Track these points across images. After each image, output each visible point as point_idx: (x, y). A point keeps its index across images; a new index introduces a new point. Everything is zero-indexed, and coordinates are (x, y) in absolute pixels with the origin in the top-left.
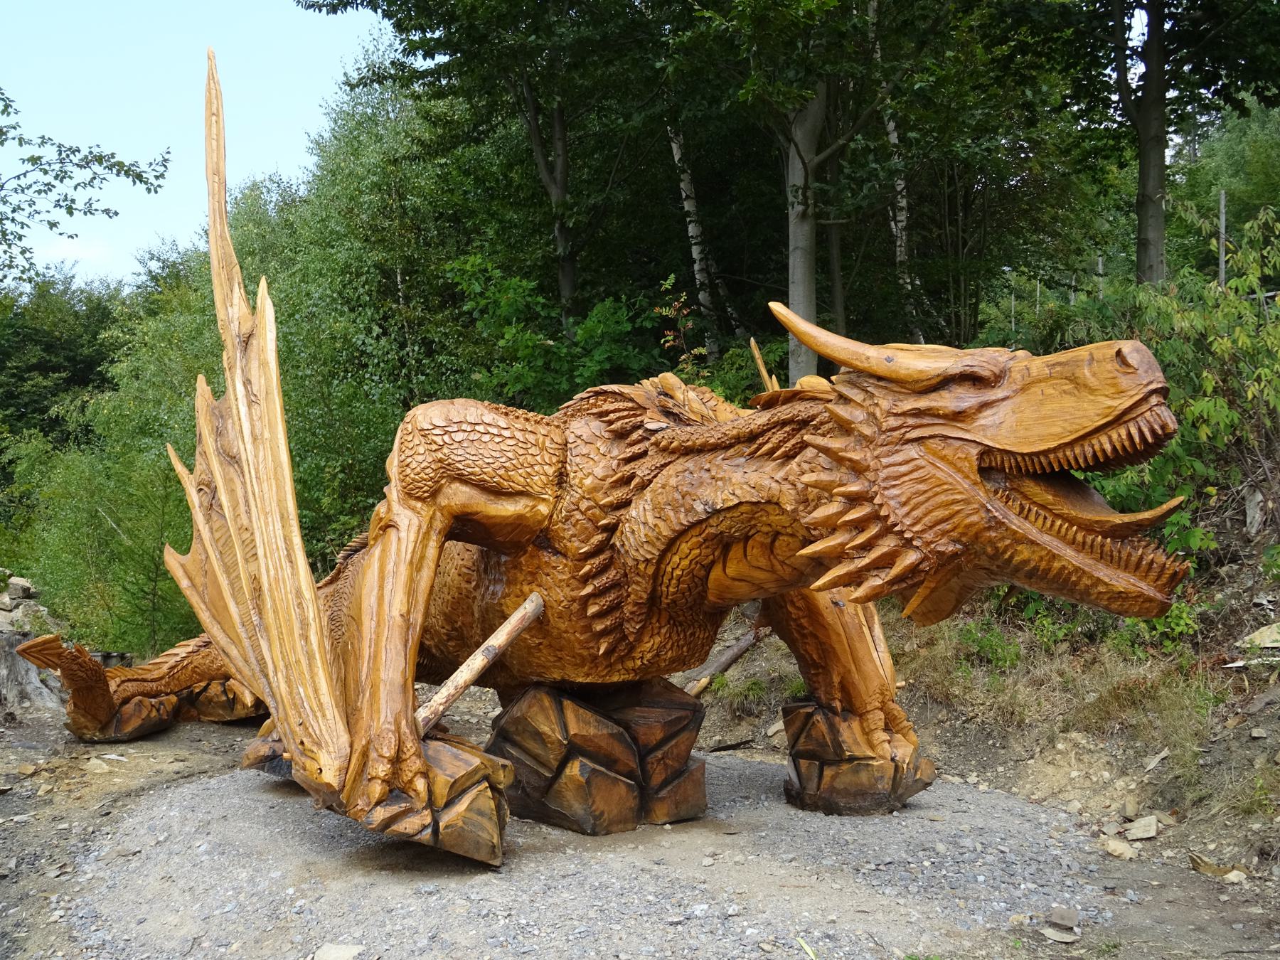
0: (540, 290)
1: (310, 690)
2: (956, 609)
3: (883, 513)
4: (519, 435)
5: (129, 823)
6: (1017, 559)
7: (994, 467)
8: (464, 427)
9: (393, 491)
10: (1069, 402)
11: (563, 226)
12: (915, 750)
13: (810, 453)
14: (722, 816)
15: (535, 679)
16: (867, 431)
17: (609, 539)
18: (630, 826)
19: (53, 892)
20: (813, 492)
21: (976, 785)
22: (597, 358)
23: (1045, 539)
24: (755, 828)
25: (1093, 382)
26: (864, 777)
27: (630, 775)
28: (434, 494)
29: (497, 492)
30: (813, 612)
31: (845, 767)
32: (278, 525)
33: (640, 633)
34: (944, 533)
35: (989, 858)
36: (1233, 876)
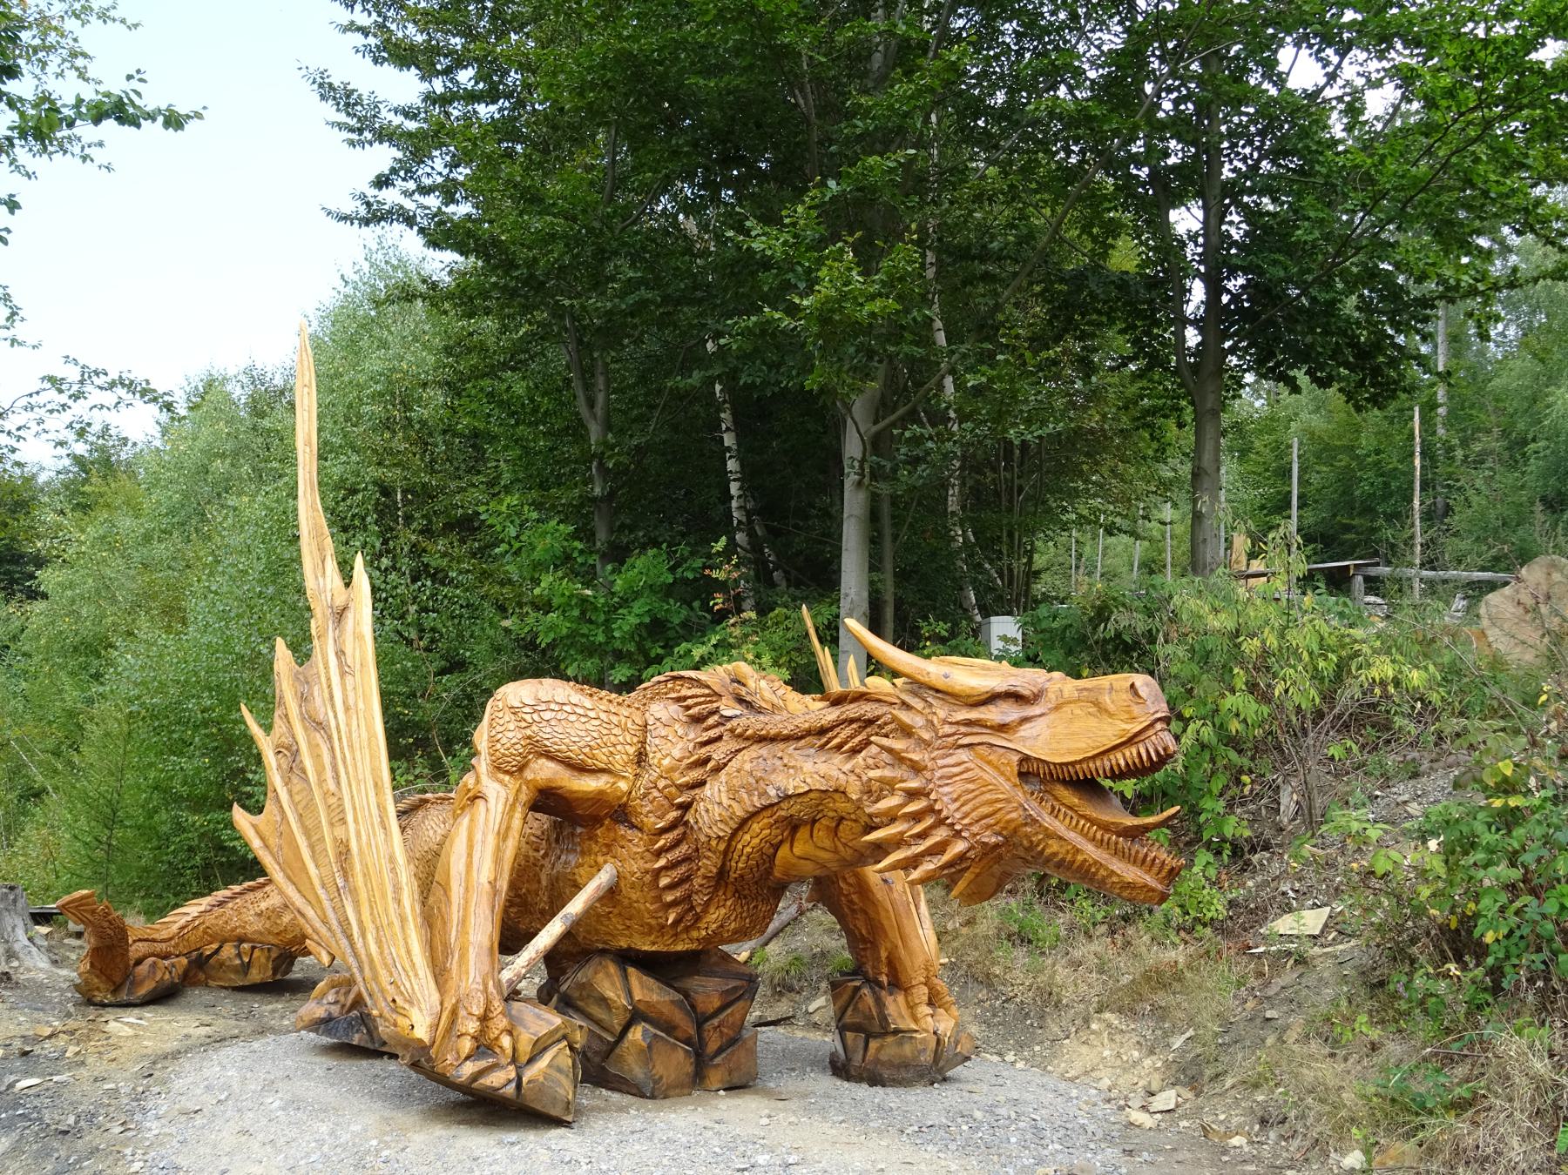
0: (575, 536)
1: (403, 952)
2: (999, 888)
3: (937, 807)
4: (603, 716)
5: (178, 1084)
6: (1048, 851)
7: (1029, 771)
8: (553, 706)
9: (482, 764)
10: (1092, 722)
11: (601, 465)
12: (957, 1024)
13: (873, 749)
14: (772, 1085)
15: (600, 946)
16: (926, 736)
17: (682, 816)
18: (686, 1091)
19: (127, 1146)
20: (875, 786)
21: (1013, 1063)
22: (636, 610)
23: (1071, 835)
24: (805, 1096)
25: (1111, 708)
26: (907, 1049)
27: (688, 1042)
28: (522, 768)
29: (581, 769)
30: (863, 889)
31: (890, 1039)
32: (372, 793)
33: (707, 904)
34: (988, 827)
35: (1022, 1125)
36: (1236, 1141)
